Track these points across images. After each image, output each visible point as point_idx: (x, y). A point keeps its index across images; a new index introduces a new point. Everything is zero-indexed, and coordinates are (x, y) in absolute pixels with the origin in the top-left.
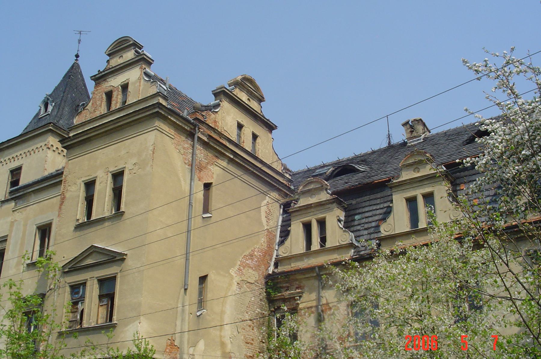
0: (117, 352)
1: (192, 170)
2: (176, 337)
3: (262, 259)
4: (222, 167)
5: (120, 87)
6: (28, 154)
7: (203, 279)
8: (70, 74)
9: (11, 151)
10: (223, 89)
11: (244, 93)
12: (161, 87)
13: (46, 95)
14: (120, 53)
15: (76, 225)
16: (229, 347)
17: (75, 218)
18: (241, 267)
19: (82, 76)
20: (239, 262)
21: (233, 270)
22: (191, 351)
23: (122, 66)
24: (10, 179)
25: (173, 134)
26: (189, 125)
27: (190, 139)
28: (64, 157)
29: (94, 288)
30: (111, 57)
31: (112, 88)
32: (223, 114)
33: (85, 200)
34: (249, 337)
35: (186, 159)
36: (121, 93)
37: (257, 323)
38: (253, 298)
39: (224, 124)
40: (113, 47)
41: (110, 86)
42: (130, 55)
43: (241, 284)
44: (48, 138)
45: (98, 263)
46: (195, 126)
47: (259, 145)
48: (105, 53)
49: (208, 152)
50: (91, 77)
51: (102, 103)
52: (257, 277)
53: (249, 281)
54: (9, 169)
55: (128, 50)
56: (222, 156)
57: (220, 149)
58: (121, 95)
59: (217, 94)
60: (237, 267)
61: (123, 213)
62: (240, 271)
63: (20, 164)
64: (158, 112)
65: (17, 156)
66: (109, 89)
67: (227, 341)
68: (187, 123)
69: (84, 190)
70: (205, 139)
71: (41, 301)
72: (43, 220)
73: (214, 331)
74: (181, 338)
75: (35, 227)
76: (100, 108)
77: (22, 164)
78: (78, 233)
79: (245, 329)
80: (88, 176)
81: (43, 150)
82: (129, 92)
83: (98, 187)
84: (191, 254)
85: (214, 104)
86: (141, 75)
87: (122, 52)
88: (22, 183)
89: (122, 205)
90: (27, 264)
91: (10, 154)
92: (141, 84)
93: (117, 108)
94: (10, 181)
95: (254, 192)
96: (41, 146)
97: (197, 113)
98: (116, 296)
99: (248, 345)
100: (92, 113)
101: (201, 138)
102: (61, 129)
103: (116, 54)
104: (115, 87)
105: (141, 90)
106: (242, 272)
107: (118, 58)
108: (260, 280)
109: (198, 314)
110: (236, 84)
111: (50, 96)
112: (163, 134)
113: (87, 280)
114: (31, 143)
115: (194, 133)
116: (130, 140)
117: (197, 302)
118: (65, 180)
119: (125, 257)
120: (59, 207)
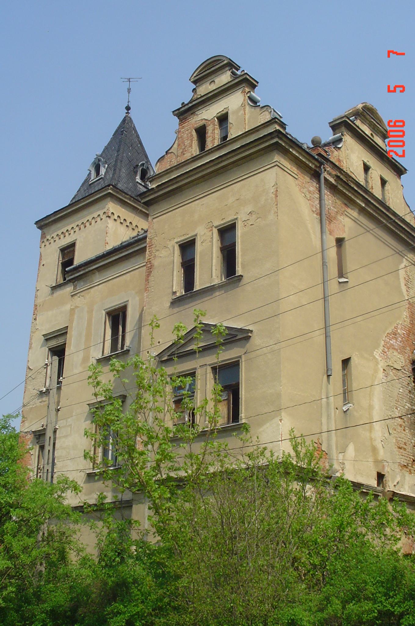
0: (272, 457)
1: (321, 220)
2: (324, 440)
3: (406, 339)
4: (353, 218)
5: (216, 119)
6: (82, 226)
7: (346, 362)
8: (122, 130)
9: (59, 225)
10: (344, 119)
11: (365, 126)
12: (275, 113)
13: (97, 155)
14: (210, 78)
15: (173, 299)
16: (381, 454)
17: (171, 291)
18: (385, 349)
19: (136, 132)
20: (383, 341)
21: (377, 352)
22: (341, 456)
23: (216, 92)
24: (61, 259)
25: (296, 173)
26: (313, 161)
27: (315, 181)
28: (127, 229)
29: (208, 379)
30: (197, 85)
31: (204, 122)
32: (347, 152)
33: (181, 267)
34: (401, 439)
35: (313, 206)
36: (218, 127)
37: (408, 422)
38: (401, 389)
39: (349, 164)
40: (200, 71)
41: (202, 120)
42: (225, 78)
43: (387, 371)
44: (107, 204)
45: (211, 346)
46: (321, 164)
47: (389, 193)
48: (190, 80)
49: (335, 198)
50: (173, 112)
51: (192, 142)
52: (404, 362)
53: (395, 367)
54: (59, 248)
55: (220, 72)
56: (352, 205)
57: (350, 195)
58: (218, 129)
59: (335, 127)
60: (382, 348)
61: (241, 277)
62: (385, 354)
63: (73, 240)
64: (277, 143)
65: (67, 230)
66: (201, 123)
67: (379, 445)
68: (311, 159)
69: (180, 254)
70: (332, 180)
71: (192, 381)
72: (114, 302)
73: (363, 432)
74: (329, 439)
75: (104, 313)
76: (190, 148)
77: (76, 240)
78: (176, 310)
79: (396, 429)
80: (183, 235)
81: (101, 219)
82: (231, 123)
83: (199, 247)
84: (332, 328)
85: (334, 138)
86: (244, 100)
87: (213, 76)
88: (77, 261)
89: (238, 268)
90: (97, 360)
91: (59, 229)
92: (246, 112)
93: (215, 146)
94: (60, 262)
95: (389, 252)
96: (99, 215)
97: (319, 148)
98: (242, 386)
99: (401, 451)
100: (179, 156)
101: (328, 180)
102: (122, 193)
103: (206, 80)
104: (209, 121)
105: (247, 119)
106: (387, 355)
107: (208, 84)
108: (407, 366)
109: (345, 408)
110: (357, 114)
111: (101, 156)
112: (285, 173)
113: (196, 369)
114: (85, 212)
115: (320, 172)
116: (239, 183)
117: (342, 392)
118: (151, 244)
119: (250, 334)
120: (146, 279)
